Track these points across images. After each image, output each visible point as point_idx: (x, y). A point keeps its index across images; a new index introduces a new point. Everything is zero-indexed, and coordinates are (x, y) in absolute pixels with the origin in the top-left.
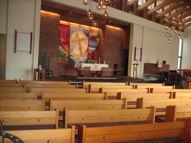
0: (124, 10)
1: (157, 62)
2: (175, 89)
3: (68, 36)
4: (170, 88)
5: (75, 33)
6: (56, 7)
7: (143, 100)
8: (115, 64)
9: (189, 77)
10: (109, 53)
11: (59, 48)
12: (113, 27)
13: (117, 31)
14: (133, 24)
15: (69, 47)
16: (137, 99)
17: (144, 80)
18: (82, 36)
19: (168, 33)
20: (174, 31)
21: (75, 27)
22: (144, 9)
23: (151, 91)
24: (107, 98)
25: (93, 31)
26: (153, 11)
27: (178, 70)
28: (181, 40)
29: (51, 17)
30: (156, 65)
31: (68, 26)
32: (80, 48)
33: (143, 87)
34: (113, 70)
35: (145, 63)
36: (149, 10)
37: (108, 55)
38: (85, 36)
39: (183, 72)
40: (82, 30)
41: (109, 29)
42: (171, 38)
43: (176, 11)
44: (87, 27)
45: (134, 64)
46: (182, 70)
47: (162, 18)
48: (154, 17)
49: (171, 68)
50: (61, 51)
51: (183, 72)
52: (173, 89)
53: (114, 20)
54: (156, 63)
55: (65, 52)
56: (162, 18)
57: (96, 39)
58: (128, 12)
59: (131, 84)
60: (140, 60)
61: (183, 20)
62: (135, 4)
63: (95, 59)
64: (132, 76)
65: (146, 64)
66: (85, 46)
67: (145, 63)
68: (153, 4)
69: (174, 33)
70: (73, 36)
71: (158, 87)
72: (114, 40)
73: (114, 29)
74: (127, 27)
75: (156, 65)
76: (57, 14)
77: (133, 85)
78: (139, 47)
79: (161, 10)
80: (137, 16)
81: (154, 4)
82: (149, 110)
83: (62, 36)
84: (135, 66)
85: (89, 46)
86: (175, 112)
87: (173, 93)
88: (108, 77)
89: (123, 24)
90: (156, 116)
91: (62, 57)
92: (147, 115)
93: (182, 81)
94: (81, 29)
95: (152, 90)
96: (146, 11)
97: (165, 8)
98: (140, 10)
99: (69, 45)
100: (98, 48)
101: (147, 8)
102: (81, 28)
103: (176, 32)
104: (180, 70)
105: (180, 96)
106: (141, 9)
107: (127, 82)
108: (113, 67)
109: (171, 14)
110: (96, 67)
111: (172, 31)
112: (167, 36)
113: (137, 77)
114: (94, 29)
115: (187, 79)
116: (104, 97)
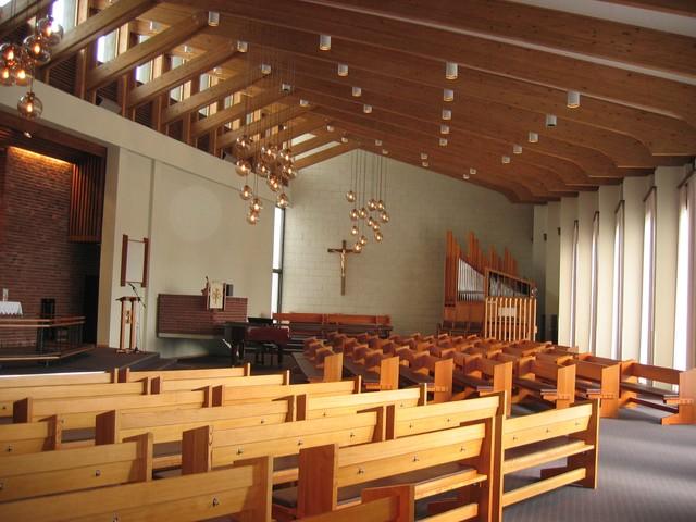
0: (82, 95)
1: (205, 291)
2: (251, 375)
4: (272, 383)
7: (210, 437)
8: (44, 301)
9: (314, 338)
10: (21, 256)
12: (38, 156)
13: (53, 170)
14: (116, 149)
16: (184, 434)
17: (162, 356)
19: (247, 188)
20: (268, 183)
22: (120, 76)
23: (215, 397)
24: (58, 440)
26: (189, 106)
27: (274, 314)
28: (278, 212)
30: (202, 300)
33: (184, 385)
34: (40, 323)
35: (160, 295)
36: (173, 102)
37: (16, 263)
39: (288, 322)
41: (22, 162)
42: (257, 207)
43: (263, 115)
45: (123, 299)
46: (285, 317)
47: (219, 134)
48: (192, 132)
49: (253, 312)
51: (288, 322)
52: (284, 383)
53: (45, 127)
54: (201, 294)
56: (219, 134)
58: (98, 103)
59: (132, 376)
60: (144, 284)
61: (284, 145)
62: (83, 51)
64: (114, 343)
65: (164, 295)
67: (160, 295)
68: (188, 85)
69: (268, 188)
71: (231, 378)
72: (41, 208)
73: (40, 162)
74: (93, 160)
75: (202, 300)
77: (144, 381)
78: (137, 236)
79: (214, 106)
80: (193, 146)
81: (190, 82)
82: (133, 445)
84: (128, 304)
86: (333, 466)
87: (298, 397)
88: (19, 354)
89: (79, 148)
90: (276, 487)
92: (244, 492)
93: (294, 354)
95: (218, 391)
96: (165, 106)
97: (228, 102)
98: (144, 100)
101: (132, 73)
103: (276, 186)
104: (279, 316)
105: (321, 406)
106: (143, 96)
107: (116, 370)
108: (39, 311)
109: (248, 123)
111: (263, 185)
112: (245, 199)
113: (134, 348)
115: (311, 345)
116: (46, 439)
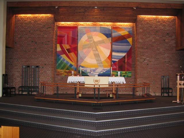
3: (74, 41)
5: (86, 35)
6: (30, 6)
11: (61, 57)
12: (154, 16)
15: (77, 55)
18: (98, 37)
21: (86, 27)
25: (119, 29)
29: (40, 20)
31: (75, 28)
32: (97, 56)
37: (146, 62)
38: (105, 37)
40: (99, 29)
44: (108, 25)
50: (65, 62)
55: (71, 62)
57: (126, 39)
63: (126, 70)
66: (105, 52)
70: (83, 40)
72: (157, 38)
76: (48, 15)
83: (66, 42)
85: (112, 51)
88: (177, 112)
91: (67, 69)
94: (97, 29)
99: (76, 52)
100: (129, 53)
102: (96, 27)
110: (97, 81)
114: (121, 25)
